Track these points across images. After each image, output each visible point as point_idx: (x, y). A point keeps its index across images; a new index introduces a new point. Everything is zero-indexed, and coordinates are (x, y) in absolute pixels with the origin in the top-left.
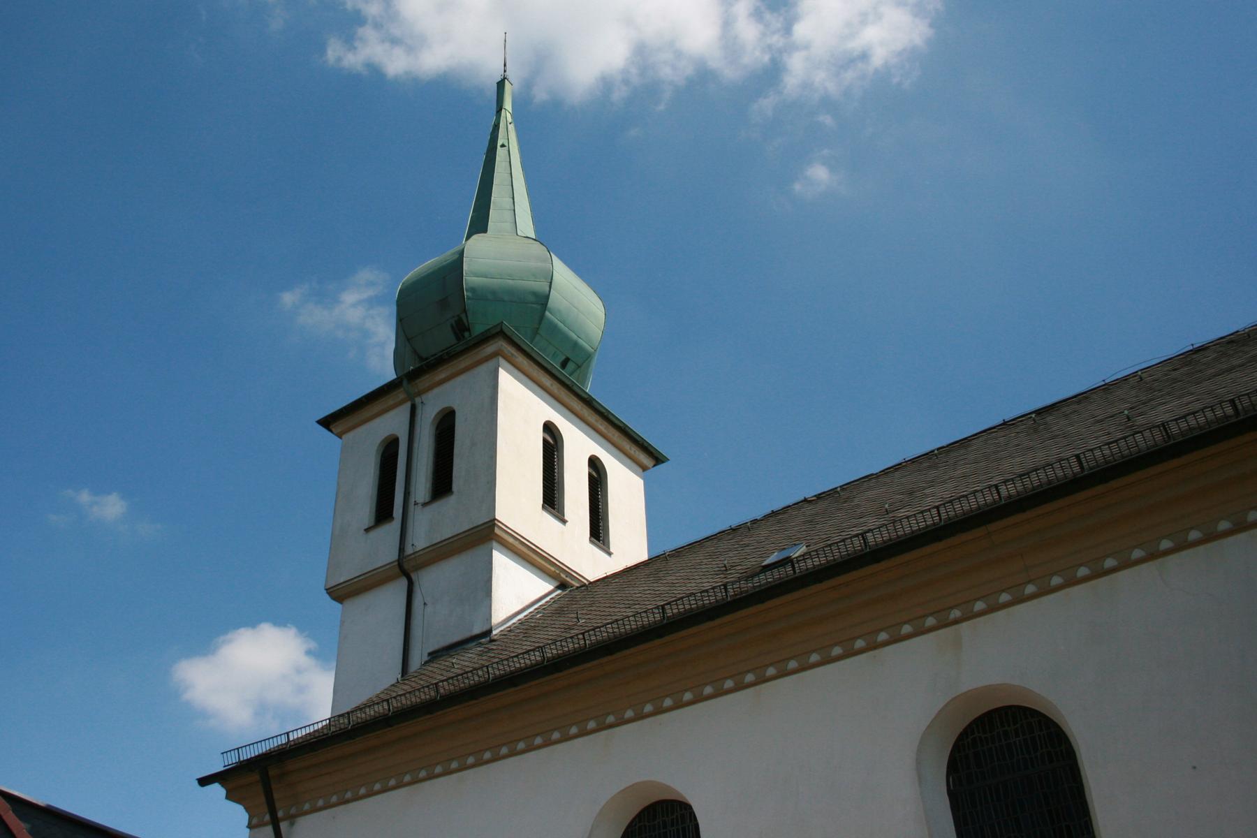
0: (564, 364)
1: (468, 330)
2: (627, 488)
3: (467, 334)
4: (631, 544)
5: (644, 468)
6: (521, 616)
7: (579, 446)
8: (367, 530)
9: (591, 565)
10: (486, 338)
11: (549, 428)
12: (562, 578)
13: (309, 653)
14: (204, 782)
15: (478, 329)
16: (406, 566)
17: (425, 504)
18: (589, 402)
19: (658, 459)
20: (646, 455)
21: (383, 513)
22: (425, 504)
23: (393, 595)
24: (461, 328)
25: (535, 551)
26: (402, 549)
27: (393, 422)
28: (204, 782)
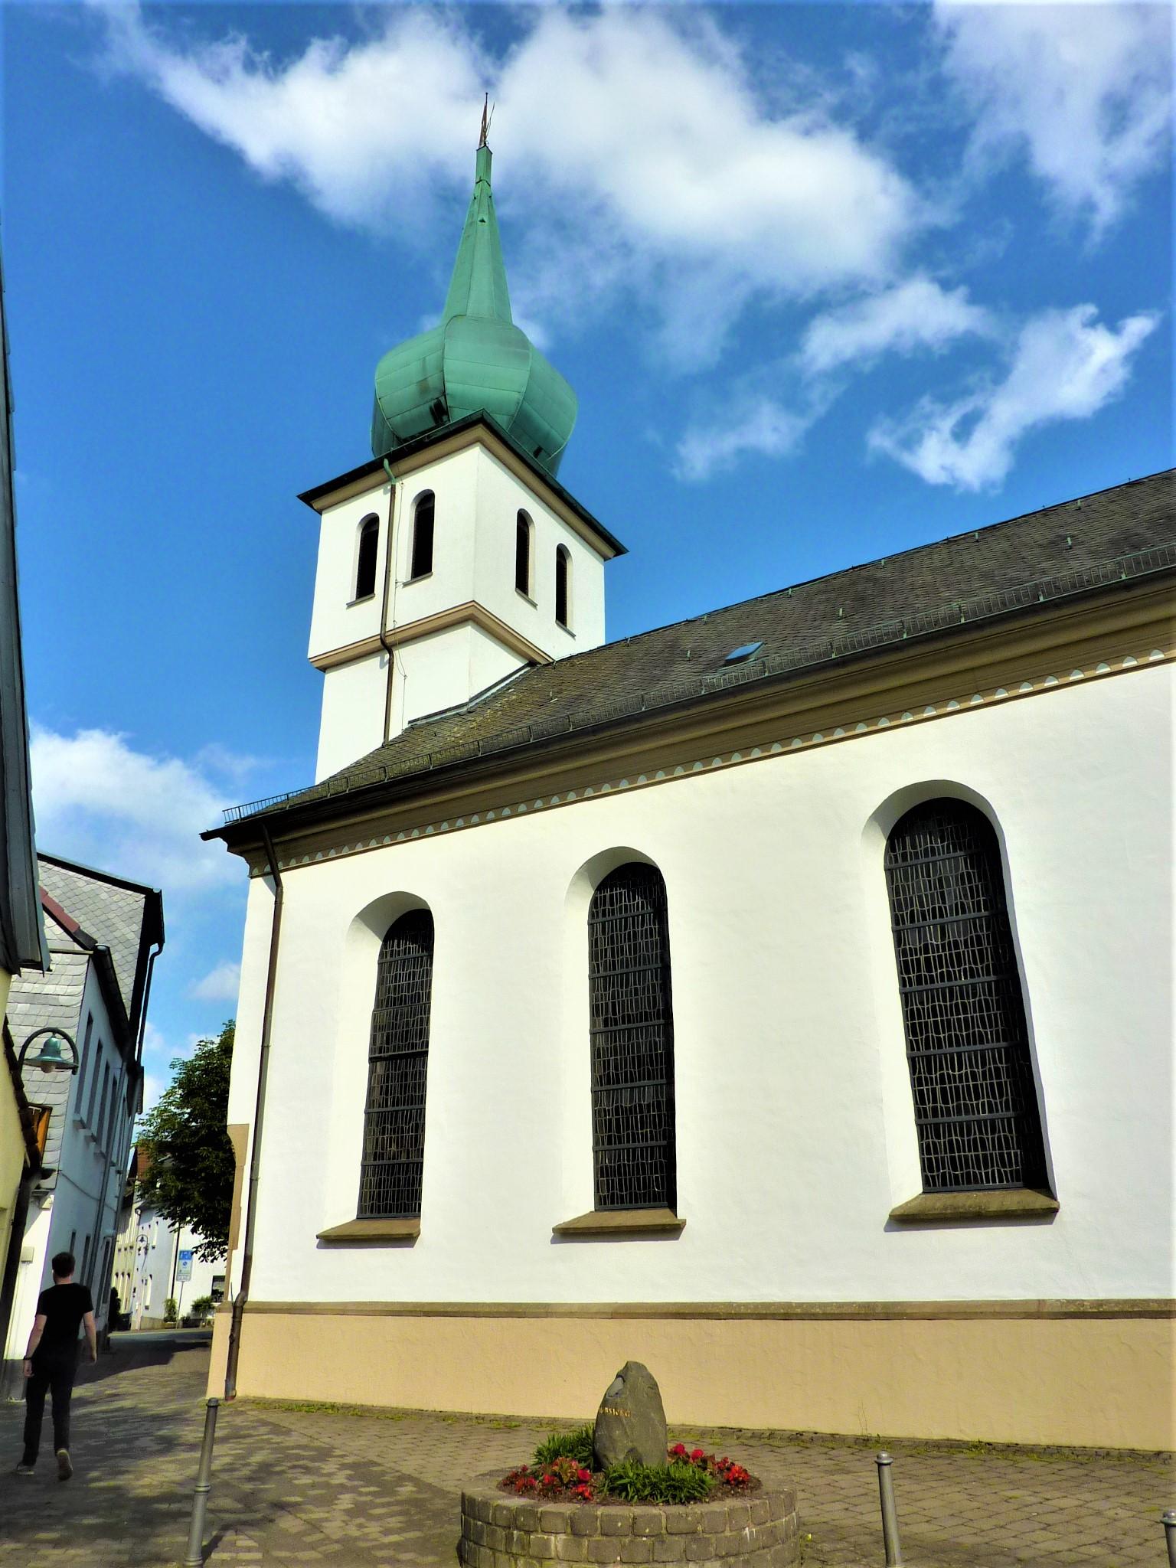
0: (537, 453)
1: (447, 413)
2: (588, 571)
3: (445, 418)
4: (589, 630)
5: (606, 558)
6: (494, 690)
7: (549, 532)
8: (350, 605)
9: (557, 646)
10: (467, 425)
11: (523, 521)
12: (534, 663)
13: (333, 69)
14: (206, 836)
15: (457, 415)
16: (388, 641)
17: (406, 585)
18: (559, 493)
19: (619, 550)
20: (609, 545)
21: (365, 587)
22: (406, 585)
23: (373, 667)
24: (439, 411)
25: (362, 468)
26: (383, 624)
27: (374, 502)
28: (206, 836)
